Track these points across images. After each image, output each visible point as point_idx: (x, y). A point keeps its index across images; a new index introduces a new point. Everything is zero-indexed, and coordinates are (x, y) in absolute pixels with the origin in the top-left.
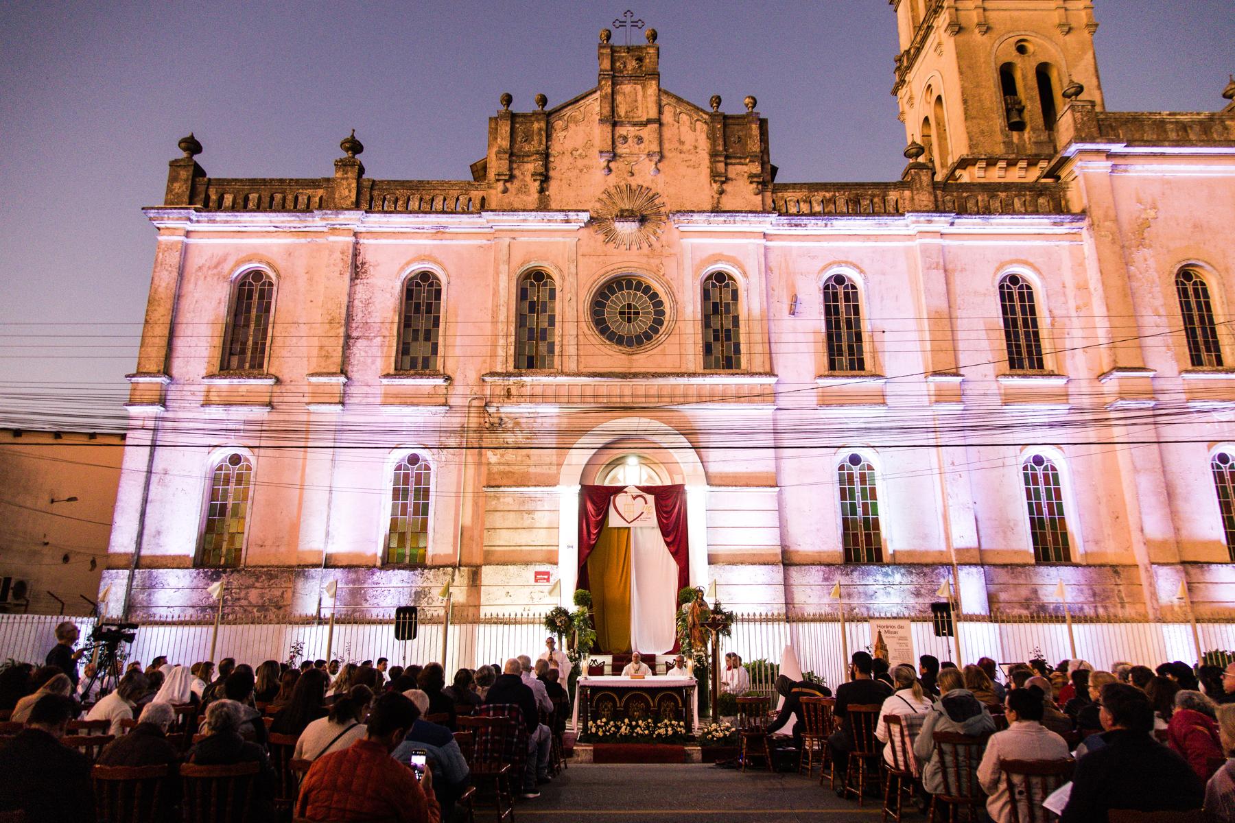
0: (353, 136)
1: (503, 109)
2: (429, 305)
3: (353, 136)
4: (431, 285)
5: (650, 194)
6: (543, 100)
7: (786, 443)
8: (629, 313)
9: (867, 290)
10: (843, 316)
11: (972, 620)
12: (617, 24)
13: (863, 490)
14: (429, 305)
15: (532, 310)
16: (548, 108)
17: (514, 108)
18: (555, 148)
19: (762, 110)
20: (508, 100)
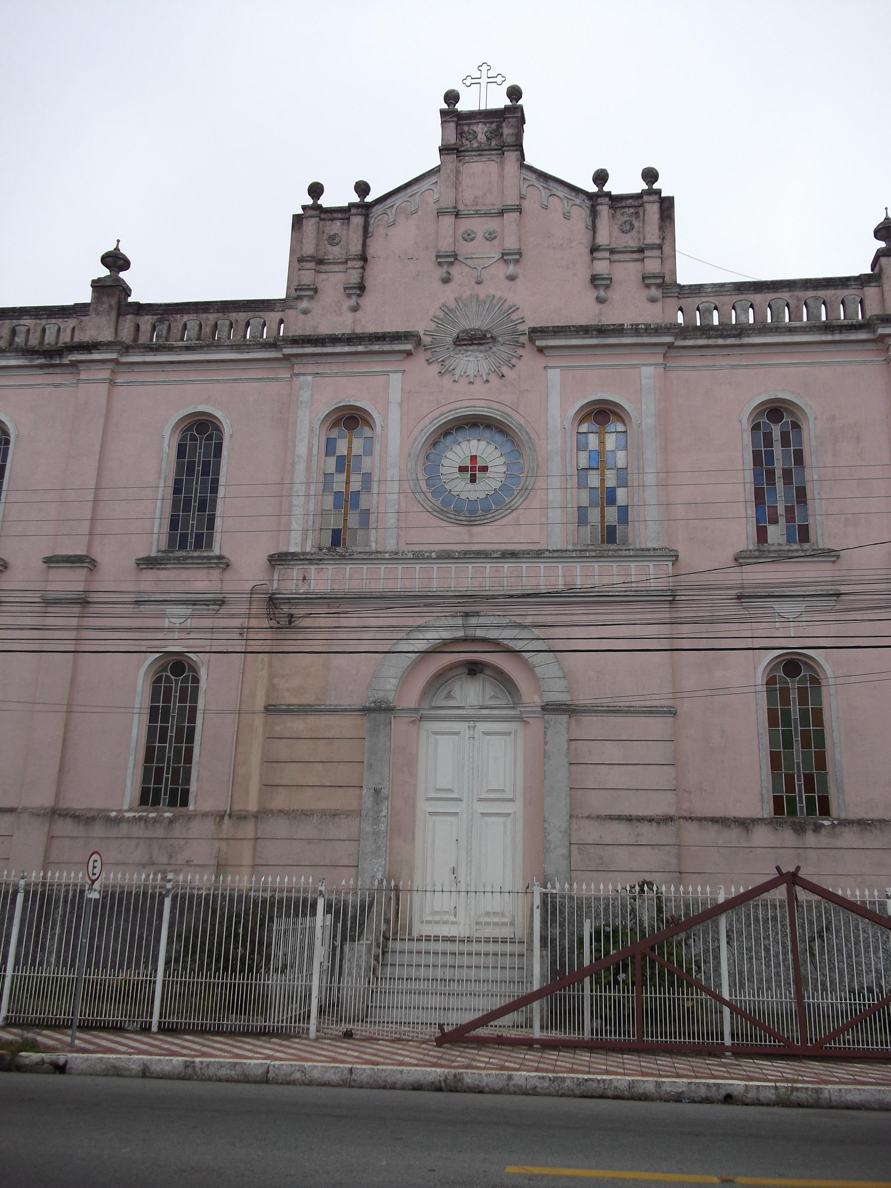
0: (117, 249)
1: (309, 201)
2: (206, 464)
3: (117, 249)
4: (210, 438)
5: (505, 307)
6: (362, 188)
7: (251, 636)
8: (473, 469)
9: (17, 437)
10: (778, 466)
11: (46, 852)
12: (469, 81)
13: (804, 713)
14: (206, 464)
15: (340, 468)
16: (369, 199)
17: (325, 201)
18: (375, 248)
19: (664, 186)
20: (316, 190)
